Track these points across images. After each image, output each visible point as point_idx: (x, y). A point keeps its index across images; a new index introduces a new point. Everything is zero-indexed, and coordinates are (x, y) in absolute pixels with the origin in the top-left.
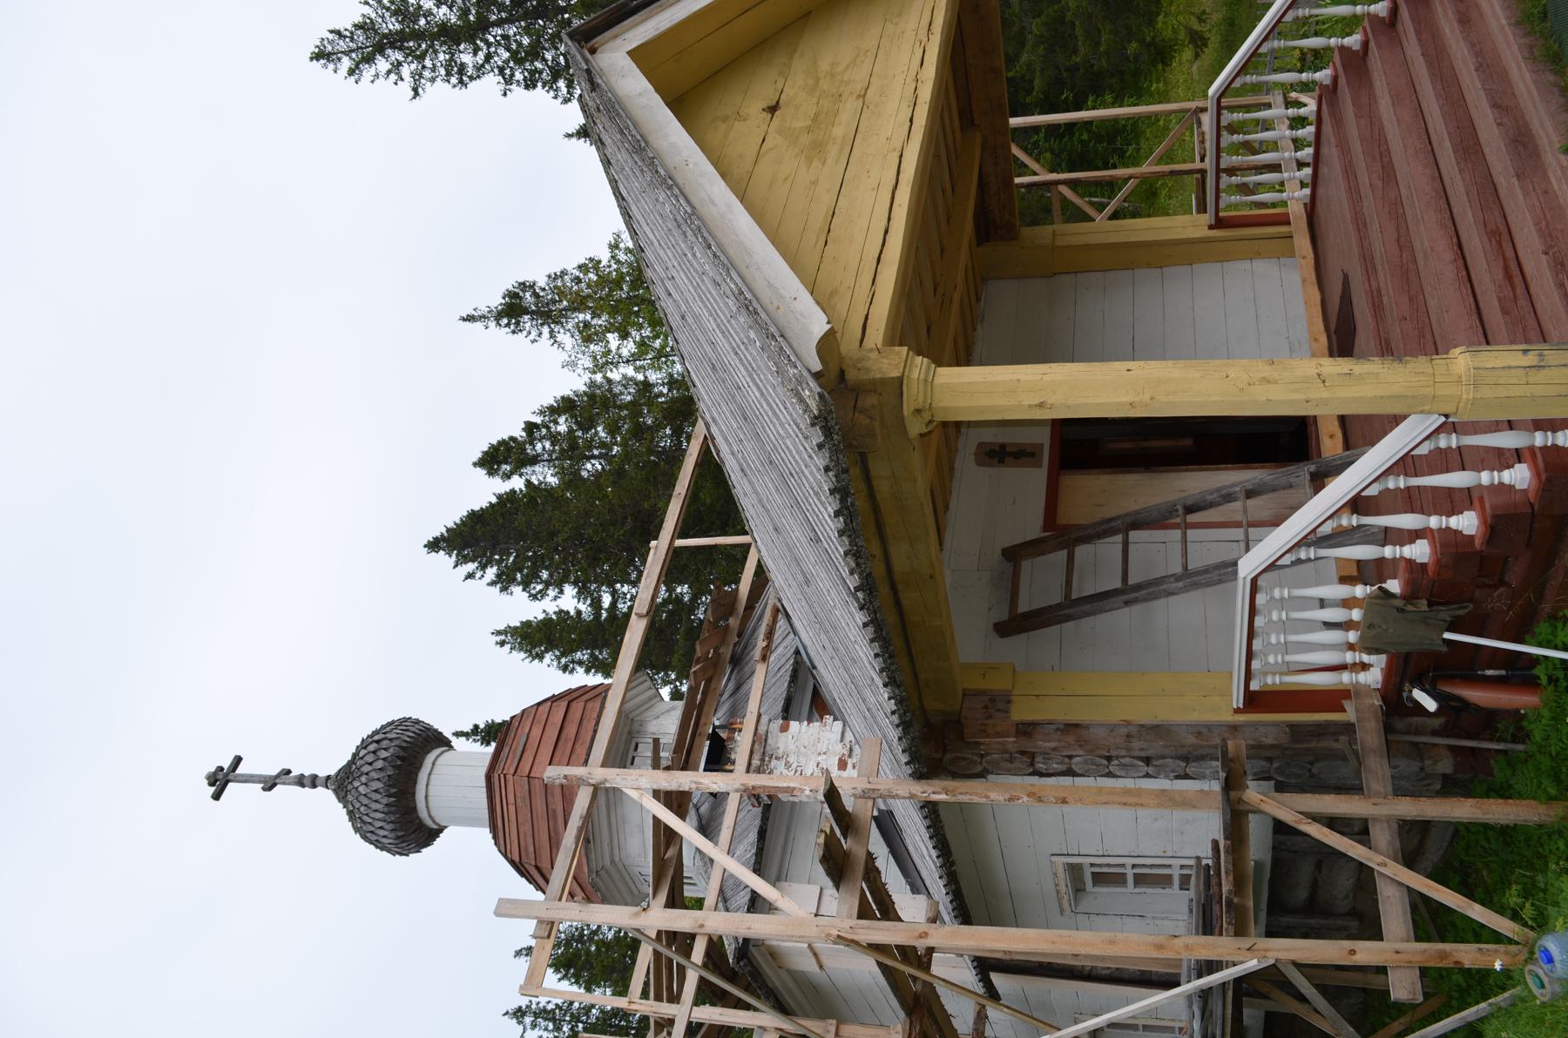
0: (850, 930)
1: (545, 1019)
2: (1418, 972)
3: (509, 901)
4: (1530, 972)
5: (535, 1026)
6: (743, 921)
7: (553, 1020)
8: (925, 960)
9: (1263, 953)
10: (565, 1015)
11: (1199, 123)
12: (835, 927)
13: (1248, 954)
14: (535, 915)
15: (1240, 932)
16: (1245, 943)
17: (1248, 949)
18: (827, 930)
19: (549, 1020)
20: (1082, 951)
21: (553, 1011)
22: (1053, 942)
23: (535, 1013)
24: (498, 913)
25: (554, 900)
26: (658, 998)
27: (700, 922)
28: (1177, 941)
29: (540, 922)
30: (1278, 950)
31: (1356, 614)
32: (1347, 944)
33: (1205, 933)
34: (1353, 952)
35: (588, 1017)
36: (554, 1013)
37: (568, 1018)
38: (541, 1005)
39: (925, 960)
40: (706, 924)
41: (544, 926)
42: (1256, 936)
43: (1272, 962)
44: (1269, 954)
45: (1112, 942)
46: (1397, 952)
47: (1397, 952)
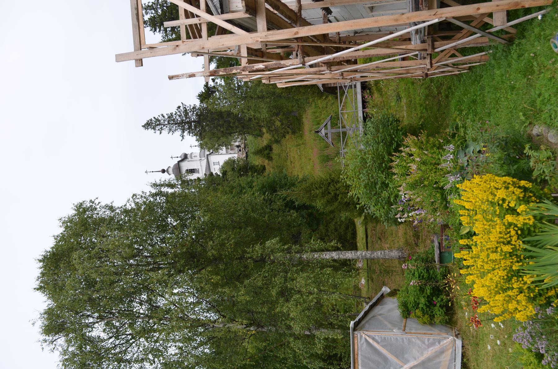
0: (265, 37)
1: (150, 10)
2: (505, 13)
3: (120, 55)
4: (552, 42)
5: (147, 13)
6: (220, 42)
7: (154, 9)
8: (299, 14)
9: (440, 16)
10: (157, 6)
11: (350, 323)
12: (259, 37)
13: (434, 17)
14: (133, 58)
15: (430, 8)
16: (432, 12)
17: (434, 15)
18: (256, 39)
19: (152, 9)
20: (364, 27)
21: (152, 5)
22: (351, 26)
23: (145, 8)
24: (117, 61)
25: (138, 50)
26: (196, 25)
27: (202, 46)
28: (404, 16)
29: (136, 60)
30: (447, 13)
31: (462, 242)
32: (476, 6)
33: (417, 11)
34: (478, 9)
35: (167, 4)
36: (153, 6)
37: (159, 7)
38: (146, 5)
39: (299, 14)
40: (205, 47)
41: (138, 61)
42: (438, 8)
43: (444, 19)
44: (443, 16)
45: (376, 22)
46: (498, 6)
47: (498, 6)
